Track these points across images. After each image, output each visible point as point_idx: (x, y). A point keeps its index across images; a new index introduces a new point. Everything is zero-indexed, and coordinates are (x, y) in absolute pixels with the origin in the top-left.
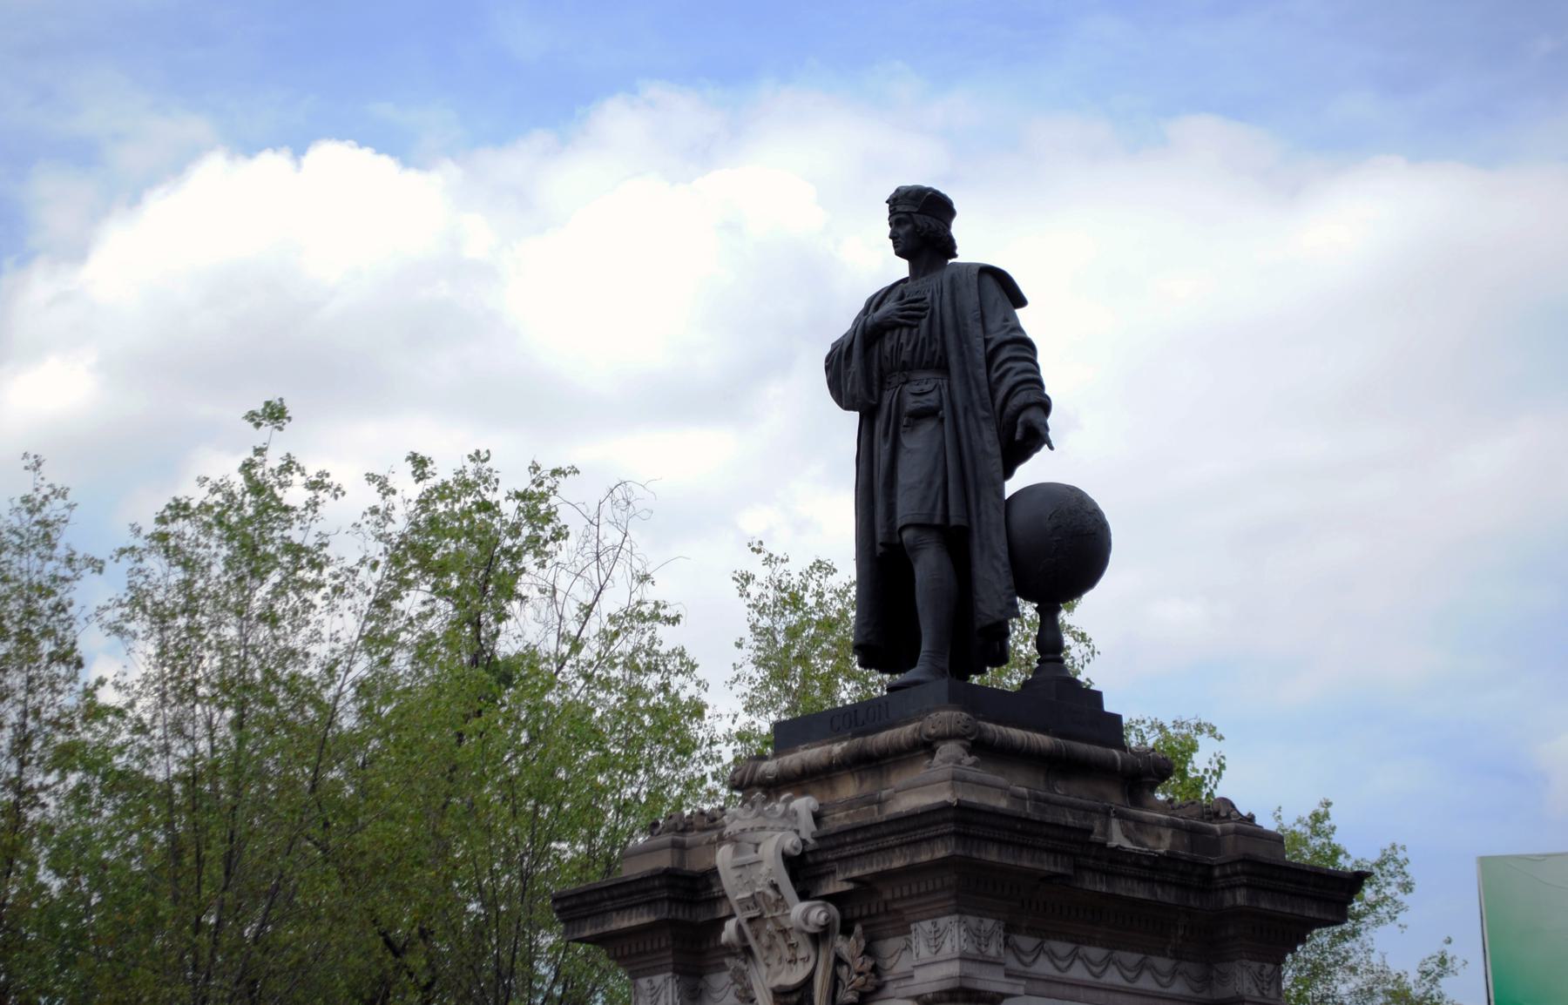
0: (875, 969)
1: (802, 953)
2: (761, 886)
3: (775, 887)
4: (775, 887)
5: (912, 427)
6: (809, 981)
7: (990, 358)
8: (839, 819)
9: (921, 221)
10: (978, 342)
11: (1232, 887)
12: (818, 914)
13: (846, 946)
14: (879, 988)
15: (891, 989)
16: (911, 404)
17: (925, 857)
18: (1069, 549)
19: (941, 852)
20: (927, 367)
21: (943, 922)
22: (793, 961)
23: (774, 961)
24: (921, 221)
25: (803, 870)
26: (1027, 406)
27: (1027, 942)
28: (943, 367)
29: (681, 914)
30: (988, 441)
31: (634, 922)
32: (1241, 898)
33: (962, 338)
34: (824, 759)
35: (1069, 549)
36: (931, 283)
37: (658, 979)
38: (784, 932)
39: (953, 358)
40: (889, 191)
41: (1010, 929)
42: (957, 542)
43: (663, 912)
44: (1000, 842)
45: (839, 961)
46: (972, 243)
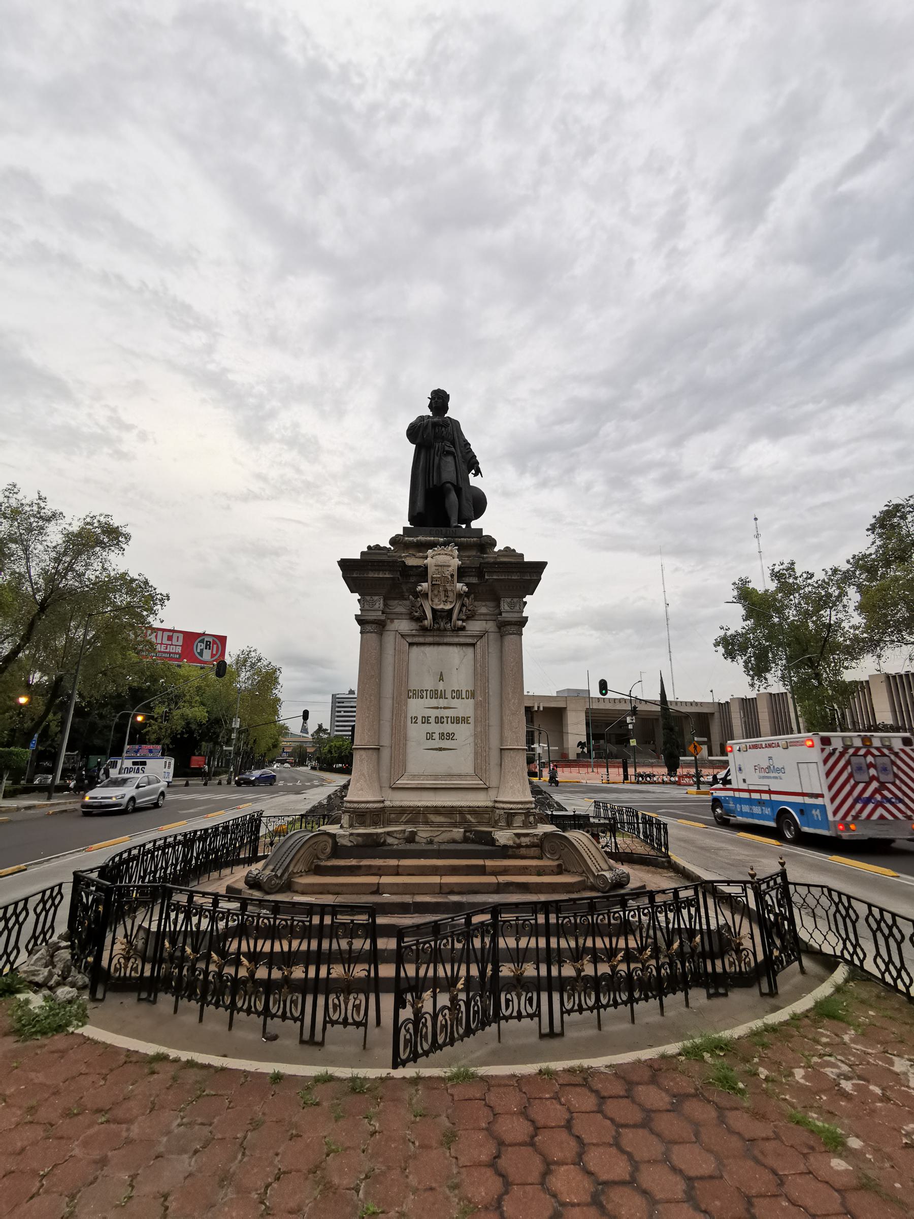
6: (452, 609)
9: (439, 400)
22: (446, 601)
38: (446, 591)
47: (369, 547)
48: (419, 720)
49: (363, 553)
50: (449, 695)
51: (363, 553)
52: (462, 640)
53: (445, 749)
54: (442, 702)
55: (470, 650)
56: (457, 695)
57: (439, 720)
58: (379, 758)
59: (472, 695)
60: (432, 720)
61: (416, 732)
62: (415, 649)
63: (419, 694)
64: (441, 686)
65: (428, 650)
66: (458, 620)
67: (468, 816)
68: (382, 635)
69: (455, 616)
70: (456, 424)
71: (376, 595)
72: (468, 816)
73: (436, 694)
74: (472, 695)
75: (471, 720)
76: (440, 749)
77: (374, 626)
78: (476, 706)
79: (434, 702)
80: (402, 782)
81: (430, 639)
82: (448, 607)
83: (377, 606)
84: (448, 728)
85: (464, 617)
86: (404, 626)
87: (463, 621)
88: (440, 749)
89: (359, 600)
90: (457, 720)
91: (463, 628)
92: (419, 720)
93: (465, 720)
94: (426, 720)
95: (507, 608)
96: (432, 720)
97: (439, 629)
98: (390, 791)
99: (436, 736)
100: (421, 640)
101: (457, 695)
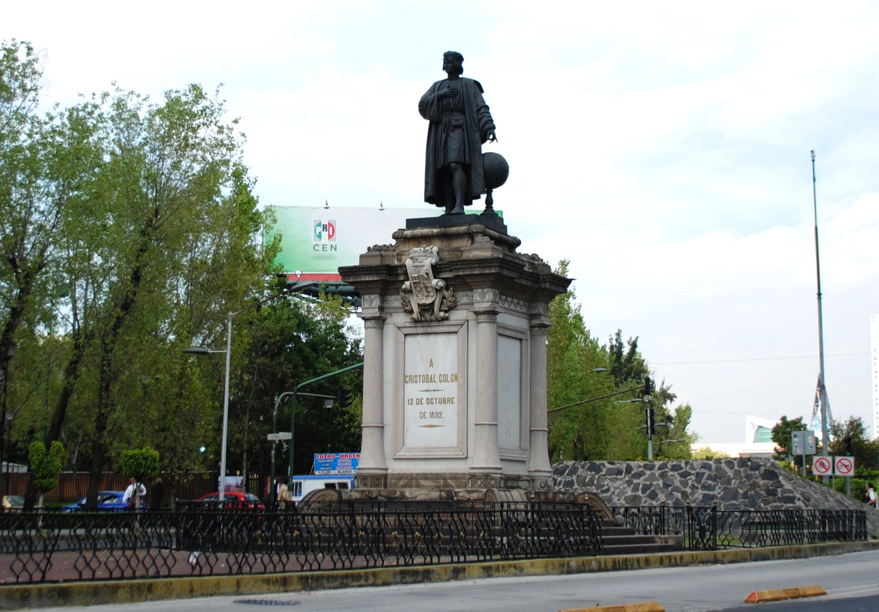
0: (455, 301)
1: (431, 294)
2: (422, 273)
3: (427, 274)
4: (427, 274)
5: (453, 131)
6: (433, 303)
7: (478, 110)
8: (447, 256)
9: (453, 62)
10: (474, 105)
11: (545, 282)
12: (441, 284)
13: (446, 294)
14: (455, 306)
15: (459, 307)
16: (454, 123)
17: (487, 271)
18: (497, 173)
19: (493, 271)
20: (458, 111)
21: (485, 290)
22: (428, 296)
23: (420, 296)
24: (453, 62)
25: (436, 270)
26: (486, 123)
27: (503, 297)
28: (463, 112)
29: (388, 278)
30: (477, 136)
31: (367, 279)
32: (547, 285)
33: (470, 104)
34: (430, 233)
35: (497, 173)
36: (453, 83)
37: (373, 296)
38: (426, 288)
39: (467, 110)
40: (446, 51)
41: (501, 294)
42: (467, 168)
43: (384, 277)
44: (507, 269)
45: (444, 297)
46: (469, 72)
47: (369, 249)
48: (414, 402)
49: (362, 257)
50: (437, 379)
51: (362, 257)
52: (445, 329)
53: (434, 426)
54: (432, 386)
55: (453, 338)
56: (444, 378)
57: (430, 401)
58: (382, 434)
59: (456, 378)
60: (424, 401)
61: (412, 412)
62: (409, 339)
63: (413, 379)
64: (431, 371)
65: (419, 338)
66: (440, 311)
67: (450, 481)
68: (382, 329)
69: (436, 308)
70: (478, 86)
71: (372, 294)
72: (450, 481)
73: (428, 379)
74: (456, 378)
75: (455, 401)
76: (431, 426)
77: (373, 322)
78: (459, 387)
79: (425, 386)
80: (402, 454)
81: (420, 330)
82: (429, 301)
83: (374, 304)
84: (437, 408)
85: (446, 308)
86: (401, 319)
87: (446, 312)
88: (431, 426)
89: (518, 243)
90: (444, 401)
91: (447, 319)
92: (414, 402)
93: (450, 400)
94: (419, 402)
95: (478, 298)
96: (424, 401)
97: (426, 321)
98: (392, 461)
99: (427, 415)
100: (414, 331)
101: (444, 378)
